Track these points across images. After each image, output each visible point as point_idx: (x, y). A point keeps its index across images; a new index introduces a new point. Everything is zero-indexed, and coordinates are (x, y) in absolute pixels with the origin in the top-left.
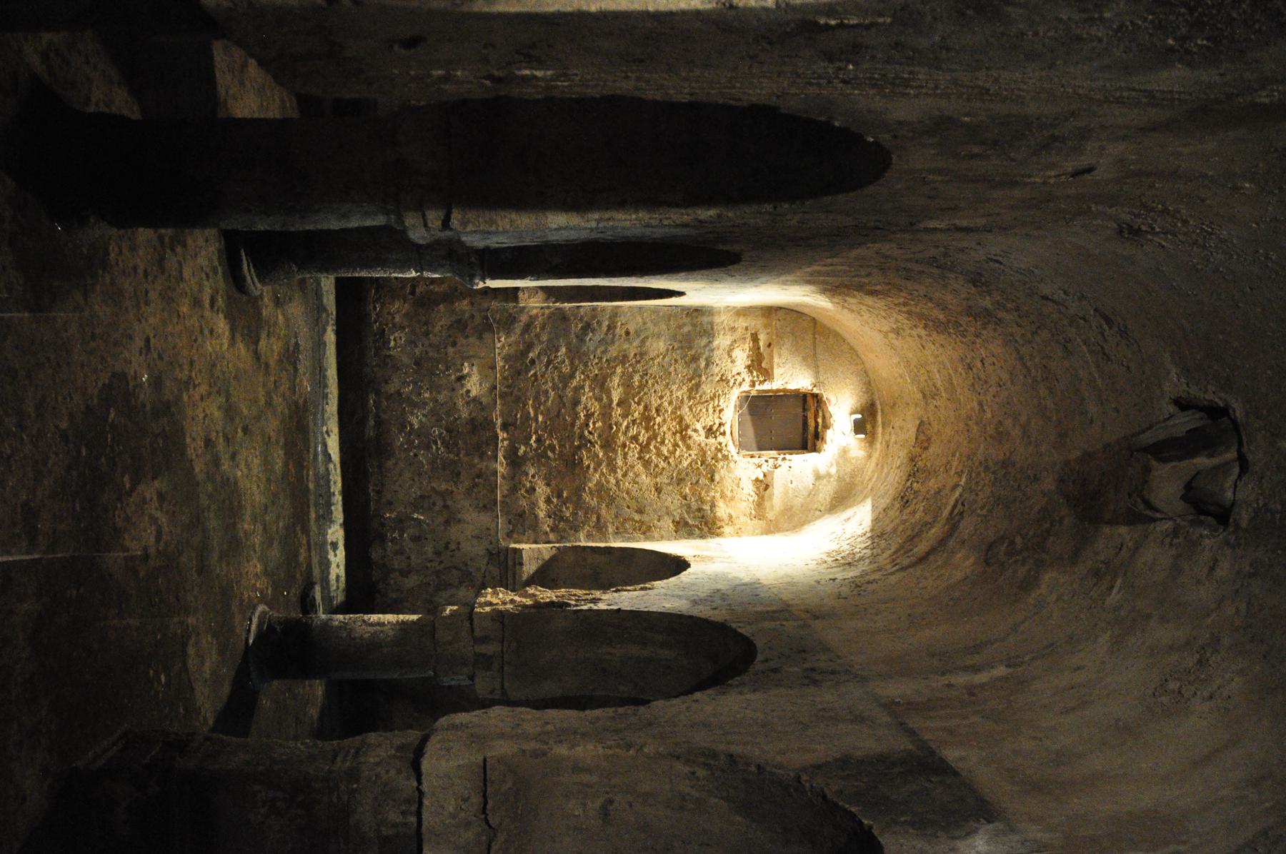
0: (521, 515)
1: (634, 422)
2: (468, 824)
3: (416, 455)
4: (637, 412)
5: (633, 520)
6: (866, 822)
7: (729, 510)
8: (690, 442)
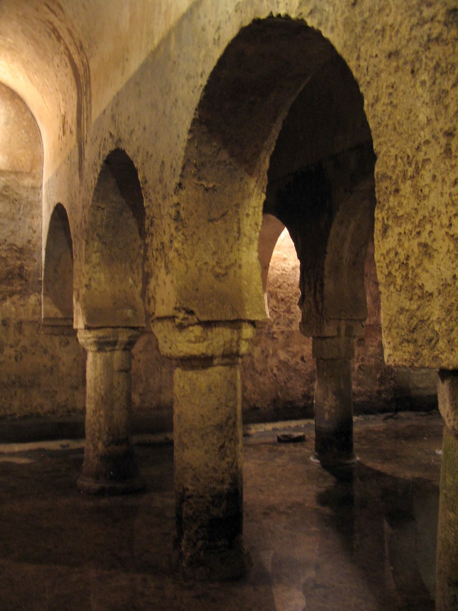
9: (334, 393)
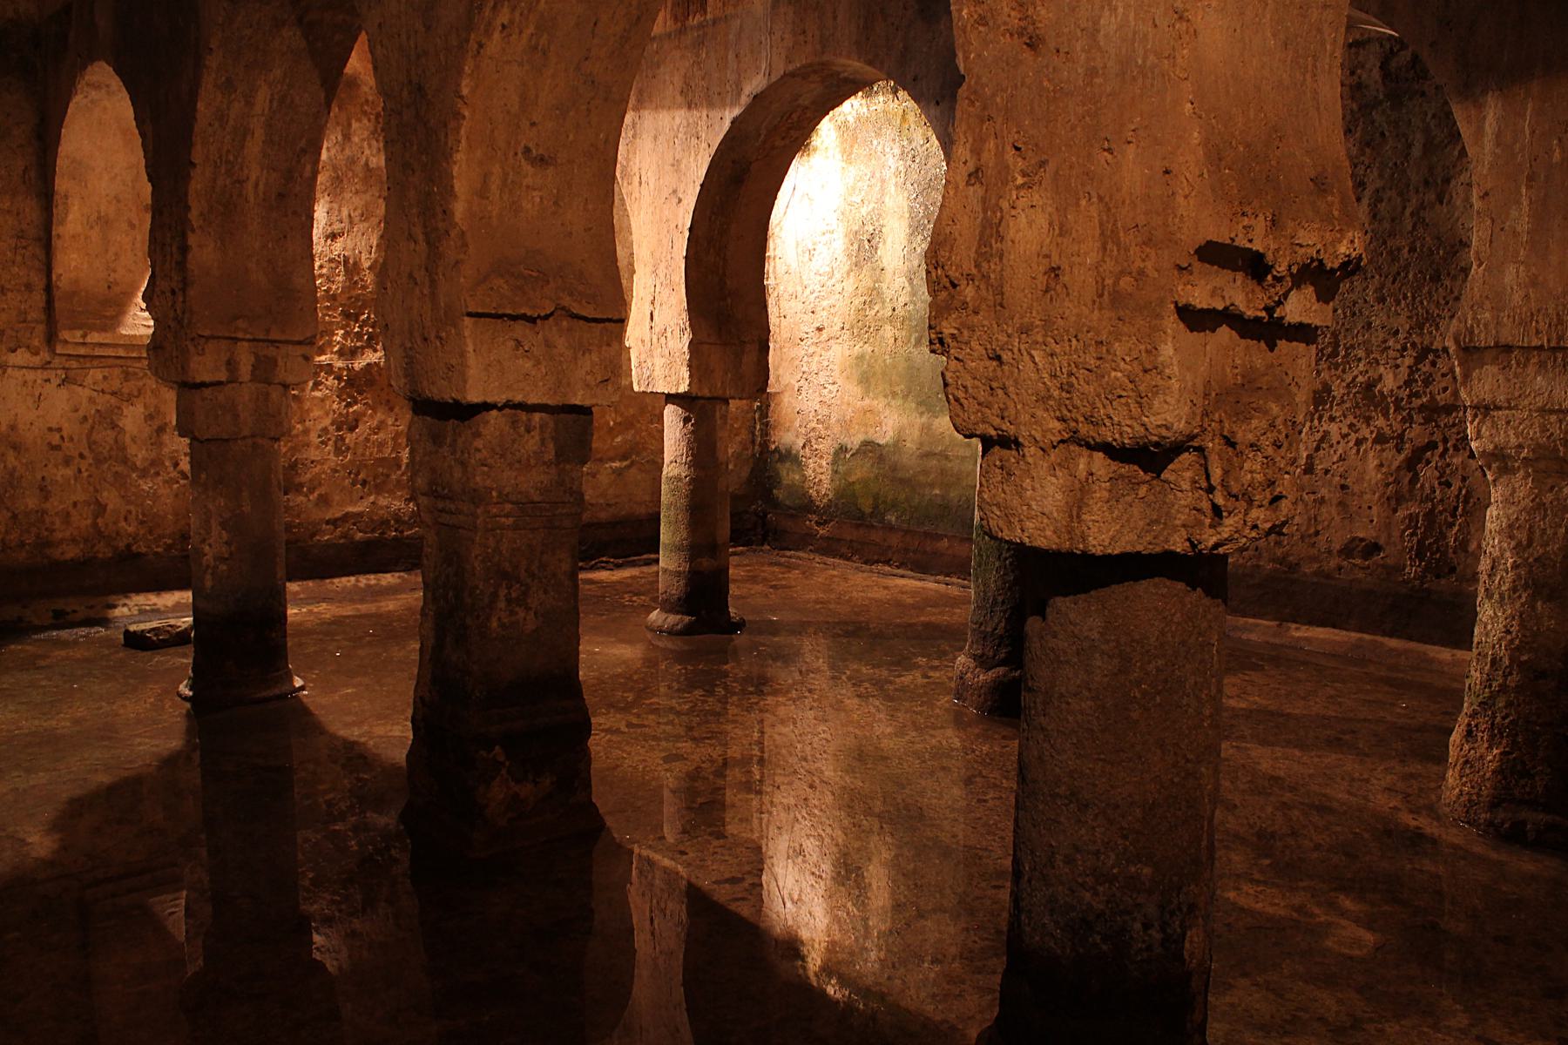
2: (548, 344)
9: (223, 525)
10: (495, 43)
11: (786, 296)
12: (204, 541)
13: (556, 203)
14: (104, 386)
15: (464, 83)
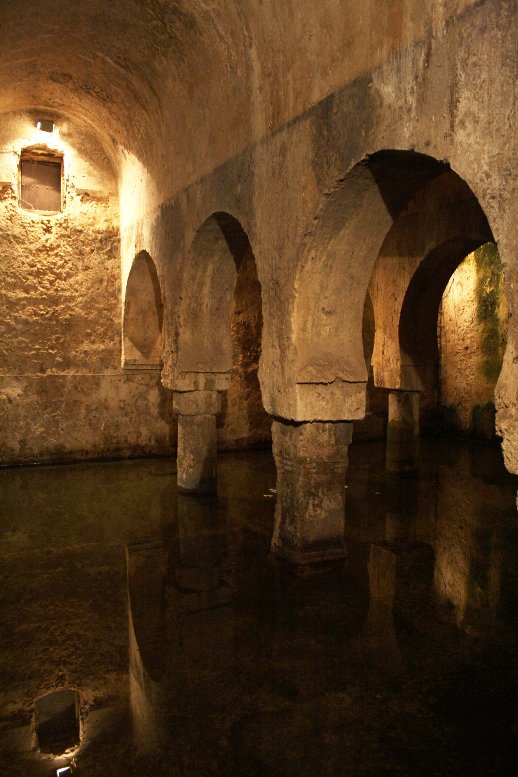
0: (102, 360)
1: (40, 283)
2: (332, 394)
3: (62, 429)
4: (33, 280)
5: (107, 286)
6: (363, 158)
7: (102, 221)
8: (55, 245)
10: (308, 266)
11: (450, 332)
12: (183, 458)
13: (336, 330)
14: (142, 382)
15: (296, 283)
